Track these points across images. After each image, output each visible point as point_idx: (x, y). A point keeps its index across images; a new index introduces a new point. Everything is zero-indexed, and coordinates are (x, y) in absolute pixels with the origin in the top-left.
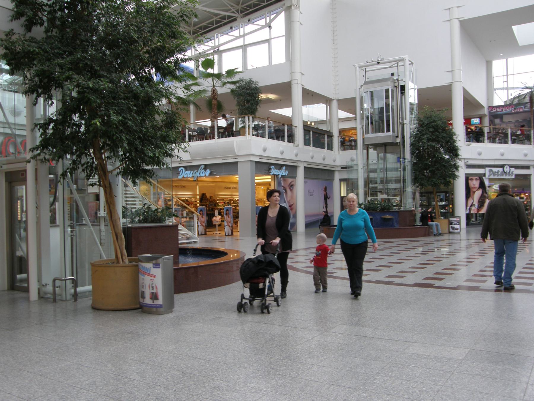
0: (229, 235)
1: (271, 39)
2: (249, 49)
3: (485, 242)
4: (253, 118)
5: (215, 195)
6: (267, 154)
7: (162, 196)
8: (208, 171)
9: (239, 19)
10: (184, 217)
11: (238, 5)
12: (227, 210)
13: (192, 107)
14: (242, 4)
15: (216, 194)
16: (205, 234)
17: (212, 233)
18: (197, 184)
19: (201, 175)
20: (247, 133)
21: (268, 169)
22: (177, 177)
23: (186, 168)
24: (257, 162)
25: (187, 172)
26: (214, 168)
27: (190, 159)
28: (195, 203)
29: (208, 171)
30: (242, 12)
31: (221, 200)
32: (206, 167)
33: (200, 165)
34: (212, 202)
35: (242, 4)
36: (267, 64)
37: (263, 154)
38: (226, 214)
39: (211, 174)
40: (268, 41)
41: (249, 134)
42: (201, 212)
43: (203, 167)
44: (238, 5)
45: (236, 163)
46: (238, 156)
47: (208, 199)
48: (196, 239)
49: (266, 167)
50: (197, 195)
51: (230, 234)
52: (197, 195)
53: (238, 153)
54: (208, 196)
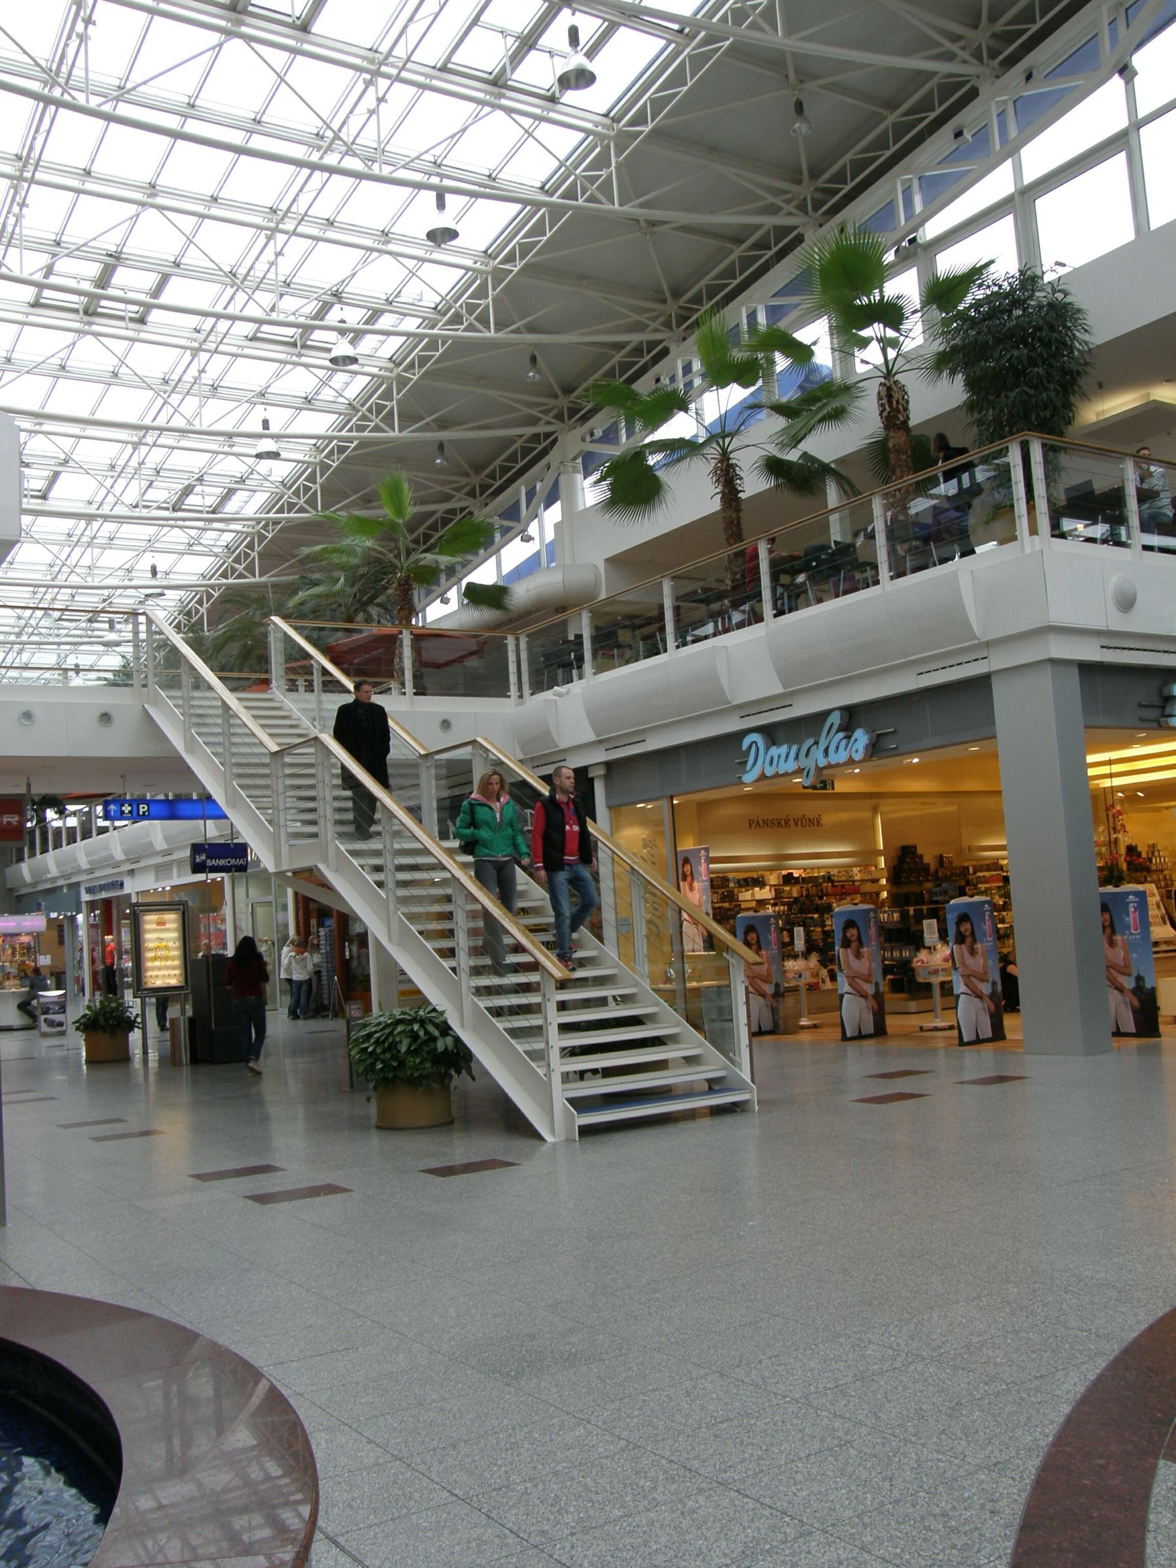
0: (978, 1041)
1: (1137, 125)
2: (1044, 205)
3: (1153, 847)
4: (1048, 449)
5: (960, 852)
6: (1139, 622)
7: (703, 868)
8: (861, 738)
9: (985, 90)
10: (795, 957)
11: (976, 27)
12: (850, 924)
13: (833, 494)
14: (993, 19)
15: (965, 845)
16: (880, 1031)
17: (915, 1021)
18: (875, 810)
19: (834, 758)
20: (1023, 524)
21: (1156, 701)
22: (740, 782)
23: (772, 734)
24: (1087, 669)
25: (774, 751)
26: (883, 722)
27: (780, 690)
28: (868, 888)
29: (861, 738)
30: (993, 54)
31: (988, 868)
32: (852, 716)
33: (825, 714)
34: (947, 879)
35: (993, 19)
36: (1128, 235)
37: (1118, 622)
38: (846, 943)
39: (875, 749)
40: (1123, 142)
41: (1033, 531)
42: (752, 937)
43: (835, 719)
44: (976, 27)
45: (982, 683)
46: (988, 644)
47: (927, 868)
48: (742, 1087)
49: (1145, 691)
50: (880, 853)
51: (987, 1032)
52: (880, 853)
53: (981, 629)
54: (929, 856)
